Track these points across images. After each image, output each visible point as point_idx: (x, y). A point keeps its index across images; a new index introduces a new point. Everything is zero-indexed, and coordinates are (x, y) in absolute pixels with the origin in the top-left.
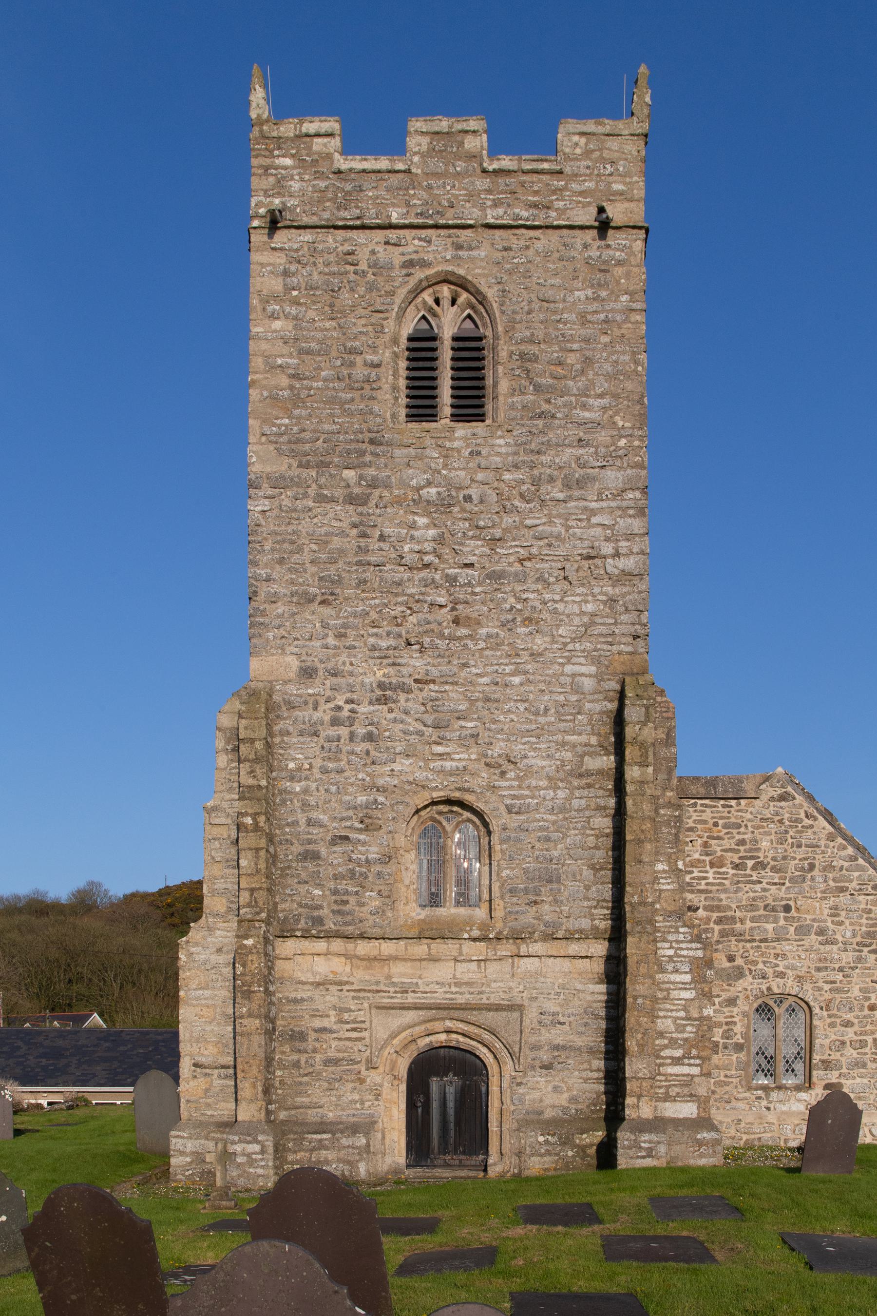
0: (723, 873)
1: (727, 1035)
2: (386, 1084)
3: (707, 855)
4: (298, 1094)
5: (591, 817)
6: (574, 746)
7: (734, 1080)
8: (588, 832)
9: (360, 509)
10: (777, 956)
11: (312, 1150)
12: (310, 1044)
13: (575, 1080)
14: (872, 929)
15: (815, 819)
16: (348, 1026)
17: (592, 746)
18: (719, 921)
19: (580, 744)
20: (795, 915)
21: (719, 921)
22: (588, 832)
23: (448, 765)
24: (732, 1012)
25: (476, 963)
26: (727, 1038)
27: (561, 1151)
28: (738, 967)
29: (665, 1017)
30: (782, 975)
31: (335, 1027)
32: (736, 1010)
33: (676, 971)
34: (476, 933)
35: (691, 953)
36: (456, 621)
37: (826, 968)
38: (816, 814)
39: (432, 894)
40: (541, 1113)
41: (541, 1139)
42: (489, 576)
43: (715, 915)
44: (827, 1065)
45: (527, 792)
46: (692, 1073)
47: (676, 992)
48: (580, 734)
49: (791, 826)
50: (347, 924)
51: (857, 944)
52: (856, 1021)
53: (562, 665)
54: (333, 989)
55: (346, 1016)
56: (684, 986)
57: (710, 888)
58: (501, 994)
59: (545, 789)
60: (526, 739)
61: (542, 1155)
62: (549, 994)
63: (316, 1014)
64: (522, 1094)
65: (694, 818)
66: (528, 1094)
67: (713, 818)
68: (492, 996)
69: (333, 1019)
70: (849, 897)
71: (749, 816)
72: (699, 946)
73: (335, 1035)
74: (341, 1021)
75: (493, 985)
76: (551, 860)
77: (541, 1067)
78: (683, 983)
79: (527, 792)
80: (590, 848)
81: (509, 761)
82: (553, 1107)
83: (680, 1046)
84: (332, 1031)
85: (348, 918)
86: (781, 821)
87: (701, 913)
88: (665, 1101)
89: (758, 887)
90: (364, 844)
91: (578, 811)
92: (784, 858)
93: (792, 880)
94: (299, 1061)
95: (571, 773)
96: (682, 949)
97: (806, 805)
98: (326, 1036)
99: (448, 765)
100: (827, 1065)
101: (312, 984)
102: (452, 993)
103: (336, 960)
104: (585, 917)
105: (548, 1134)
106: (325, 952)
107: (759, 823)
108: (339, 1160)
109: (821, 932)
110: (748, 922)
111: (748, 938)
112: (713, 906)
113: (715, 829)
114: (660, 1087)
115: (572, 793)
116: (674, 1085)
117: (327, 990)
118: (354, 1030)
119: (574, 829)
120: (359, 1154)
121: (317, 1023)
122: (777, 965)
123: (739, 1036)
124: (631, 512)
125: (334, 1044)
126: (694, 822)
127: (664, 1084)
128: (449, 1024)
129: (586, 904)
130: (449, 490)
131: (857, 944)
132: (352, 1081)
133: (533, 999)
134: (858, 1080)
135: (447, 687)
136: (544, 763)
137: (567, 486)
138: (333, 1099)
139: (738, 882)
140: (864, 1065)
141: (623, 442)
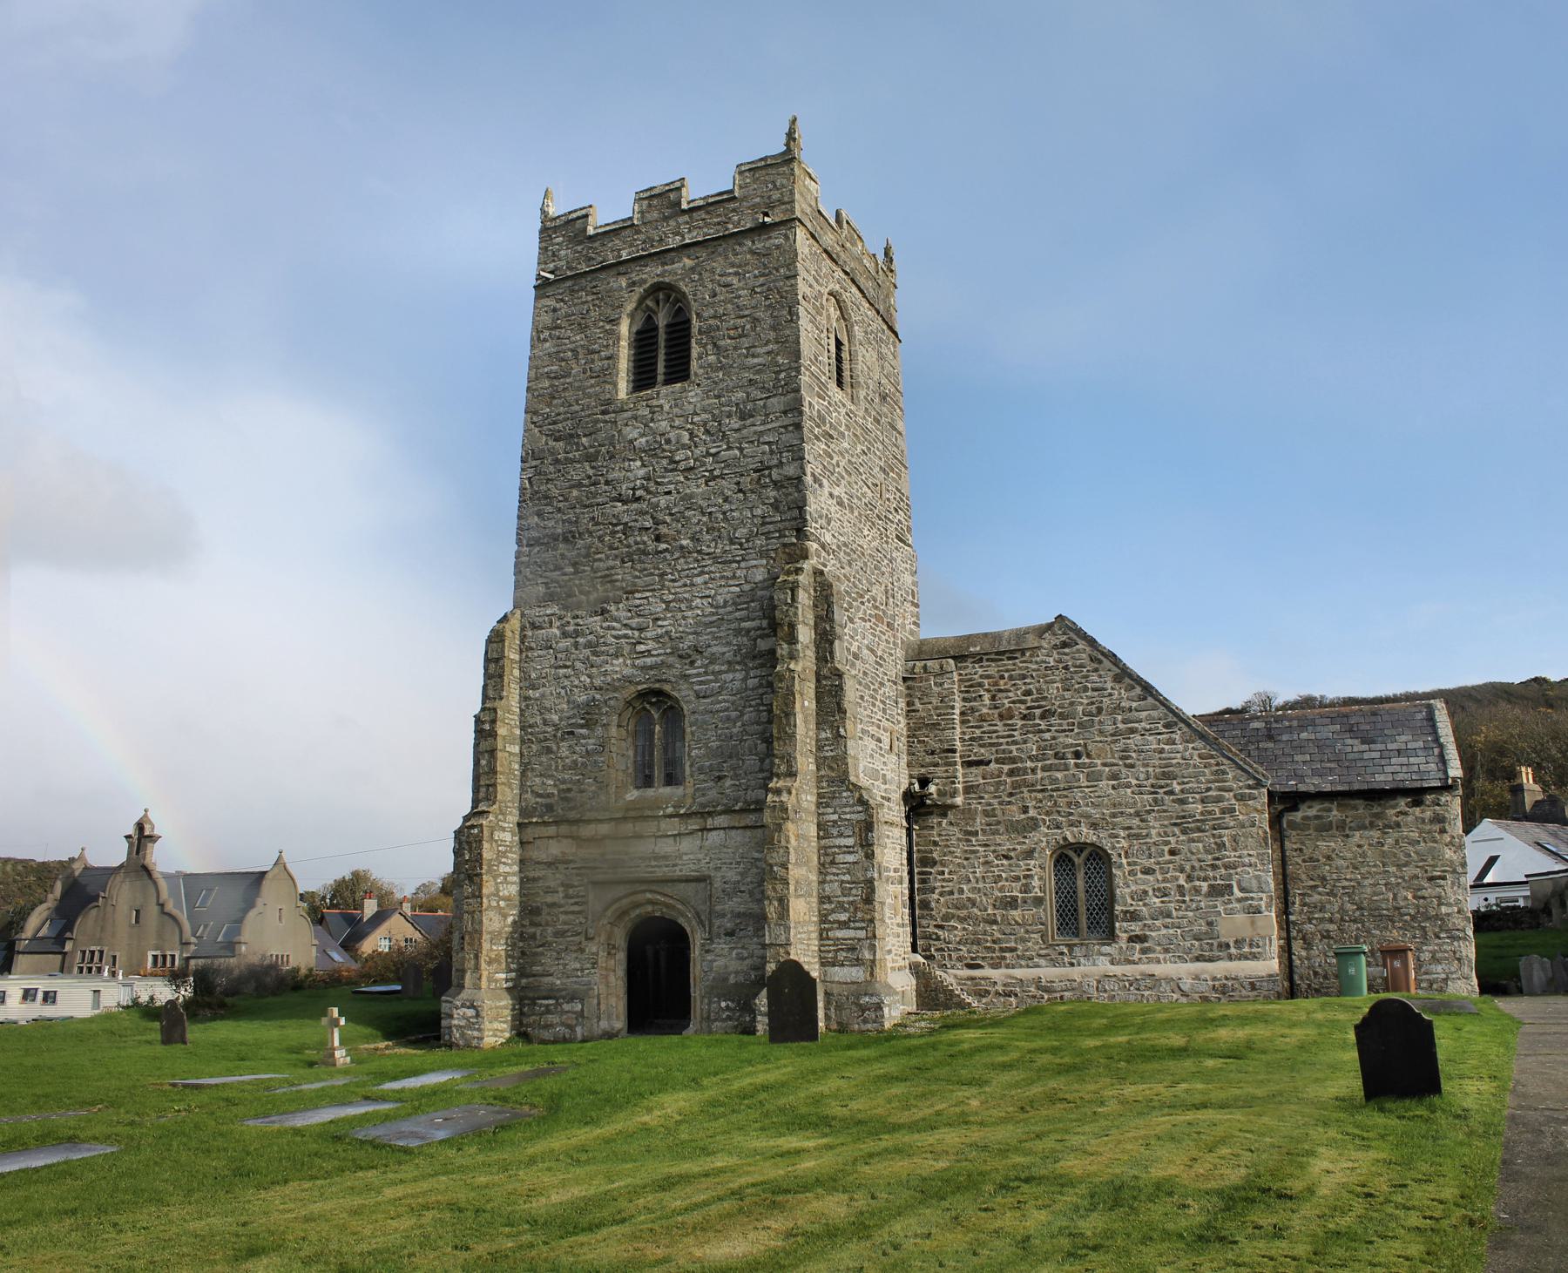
0: (1012, 725)
1: (1026, 889)
2: (601, 953)
3: (996, 708)
4: (534, 964)
5: (763, 694)
6: (748, 631)
7: (1035, 936)
8: (761, 708)
9: (593, 464)
10: (1069, 804)
11: (542, 1014)
12: (544, 918)
13: (755, 946)
14: (1165, 770)
15: (1100, 662)
16: (573, 901)
17: (764, 629)
18: (1011, 773)
19: (754, 629)
20: (1087, 761)
21: (1011, 773)
22: (761, 708)
23: (649, 661)
24: (1029, 865)
25: (672, 838)
26: (1025, 892)
27: (740, 1016)
28: (1032, 818)
29: (831, 881)
30: (1076, 824)
31: (562, 902)
32: (1033, 862)
33: (841, 835)
34: (670, 810)
35: (854, 816)
36: (658, 539)
37: (1122, 813)
38: (1100, 657)
39: (646, 776)
40: (726, 979)
41: (723, 1004)
42: (682, 499)
43: (1006, 768)
44: (1133, 916)
45: (712, 677)
46: (858, 936)
47: (841, 856)
48: (754, 620)
49: (1076, 672)
50: (571, 809)
51: (1152, 786)
52: (1156, 867)
53: (738, 562)
54: (561, 867)
55: (571, 891)
56: (849, 850)
57: (1001, 740)
58: (691, 865)
59: (726, 672)
60: (709, 630)
61: (724, 1020)
62: (731, 864)
63: (549, 891)
64: (710, 961)
65: (980, 673)
66: (715, 961)
67: (999, 671)
68: (684, 867)
69: (561, 895)
70: (1140, 737)
71: (1034, 667)
72: (860, 809)
73: (562, 910)
74: (567, 896)
75: (685, 857)
76: (731, 737)
77: (726, 935)
78: (847, 847)
79: (712, 677)
80: (764, 723)
81: (697, 651)
82: (737, 973)
83: (846, 910)
84: (560, 906)
85: (572, 804)
86: (1066, 668)
87: (993, 766)
88: (834, 965)
89: (1047, 736)
90: (584, 737)
91: (753, 689)
92: (1072, 704)
93: (1081, 725)
94: (535, 934)
95: (746, 656)
96: (845, 813)
97: (1088, 649)
98: (555, 911)
99: (649, 661)
100: (1133, 916)
101: (545, 863)
102: (652, 867)
103: (565, 841)
104: (760, 788)
105: (729, 1000)
106: (555, 835)
107: (1044, 672)
108: (563, 1024)
109: (1114, 777)
110: (1039, 771)
111: (1039, 787)
112: (1004, 759)
113: (1002, 682)
114: (829, 952)
115: (747, 674)
116: (842, 949)
117: (557, 868)
118: (576, 903)
119: (750, 706)
120: (576, 1019)
121: (549, 899)
122: (1071, 814)
123: (1037, 890)
124: (791, 428)
125: (562, 917)
126: (981, 677)
127: (832, 948)
128: (649, 896)
129: (760, 776)
130: (655, 437)
131: (1152, 786)
132: (575, 951)
133: (718, 869)
134: (1164, 931)
135: (648, 594)
136: (725, 649)
137: (742, 418)
138: (561, 967)
139: (1028, 732)
140: (1169, 916)
141: (782, 375)
